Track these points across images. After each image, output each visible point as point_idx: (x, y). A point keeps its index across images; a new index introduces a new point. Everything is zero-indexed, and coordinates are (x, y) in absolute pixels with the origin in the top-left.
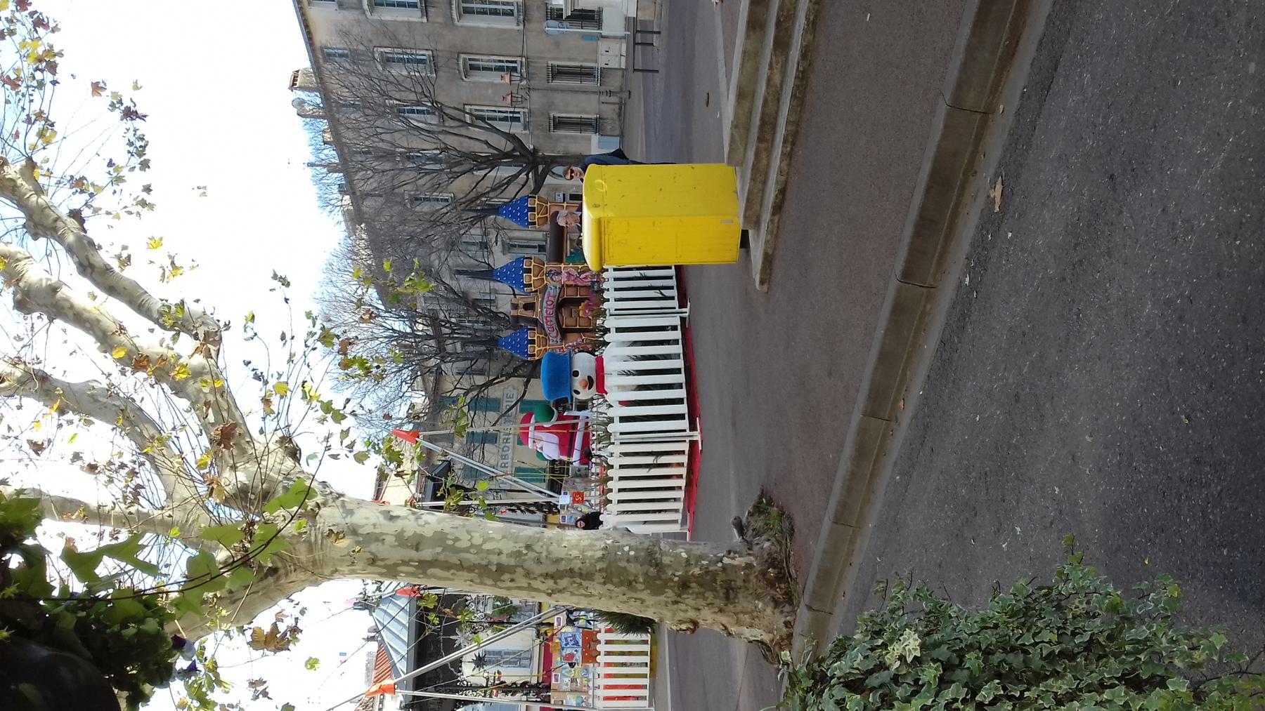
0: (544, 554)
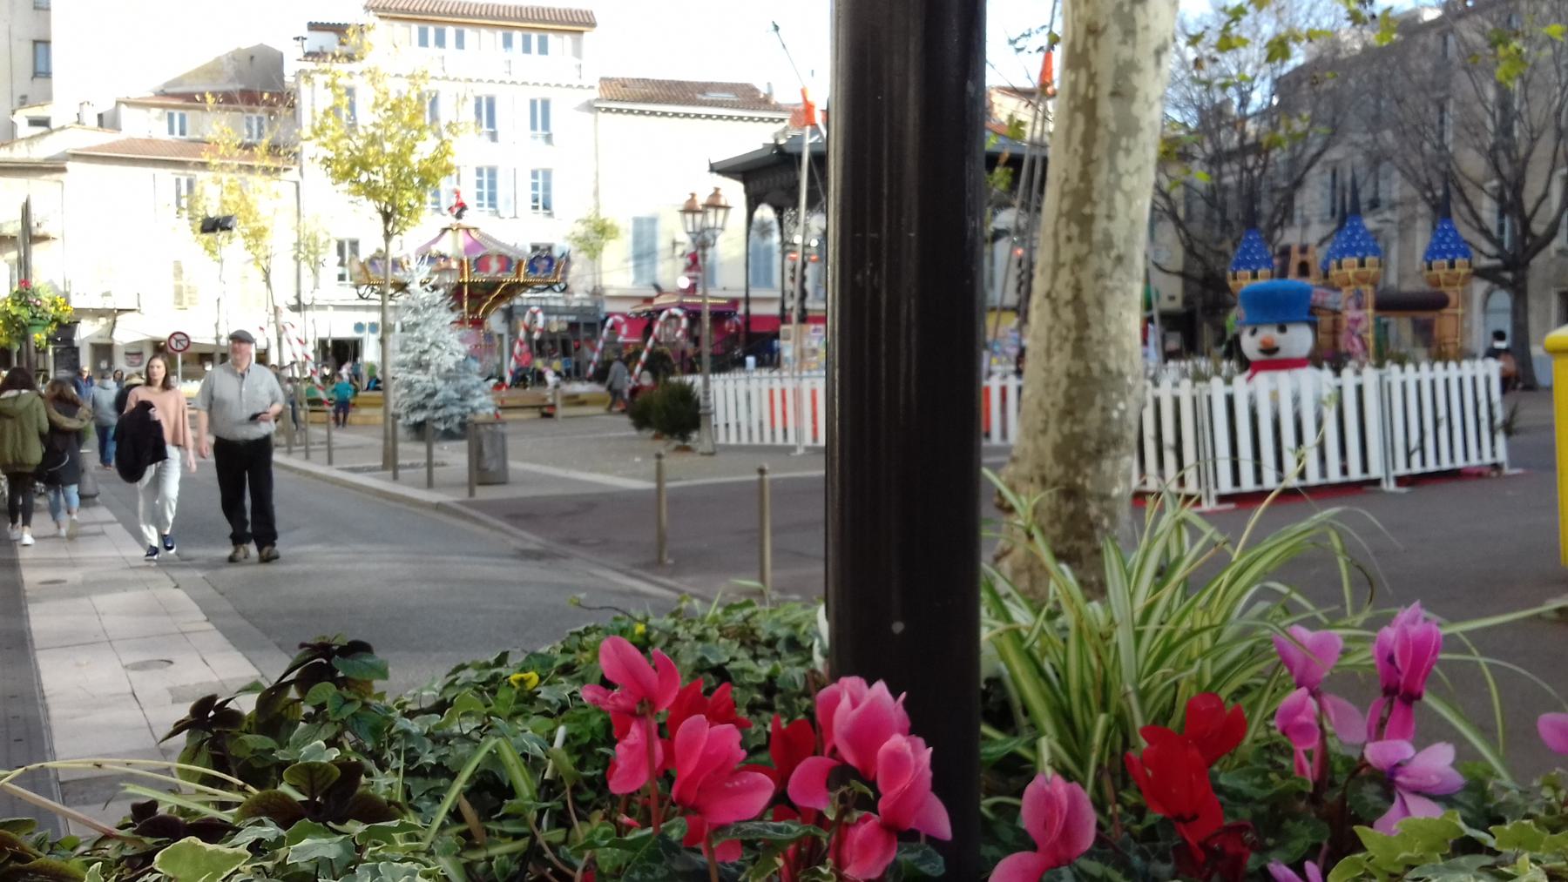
0: (1109, 283)
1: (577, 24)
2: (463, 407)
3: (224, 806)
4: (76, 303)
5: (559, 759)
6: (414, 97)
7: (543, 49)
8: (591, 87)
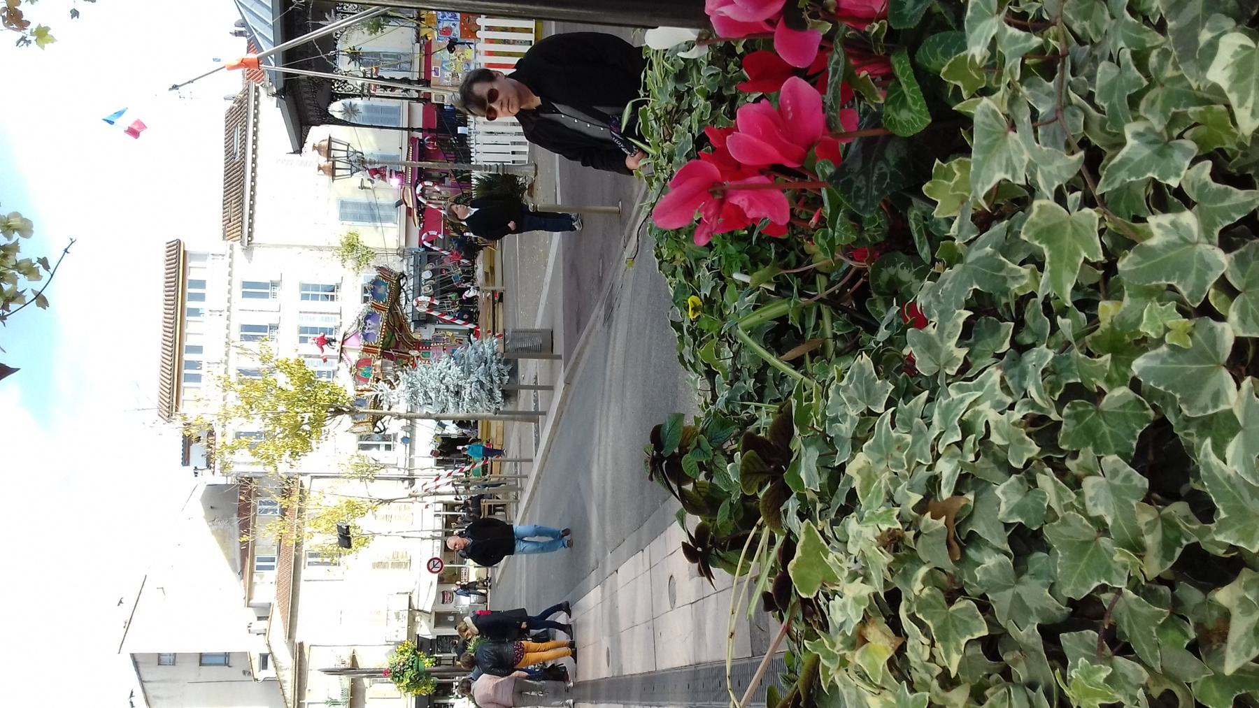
1: (178, 256)
2: (492, 362)
3: (772, 541)
4: (403, 636)
5: (761, 279)
6: (240, 387)
7: (201, 284)
8: (231, 248)
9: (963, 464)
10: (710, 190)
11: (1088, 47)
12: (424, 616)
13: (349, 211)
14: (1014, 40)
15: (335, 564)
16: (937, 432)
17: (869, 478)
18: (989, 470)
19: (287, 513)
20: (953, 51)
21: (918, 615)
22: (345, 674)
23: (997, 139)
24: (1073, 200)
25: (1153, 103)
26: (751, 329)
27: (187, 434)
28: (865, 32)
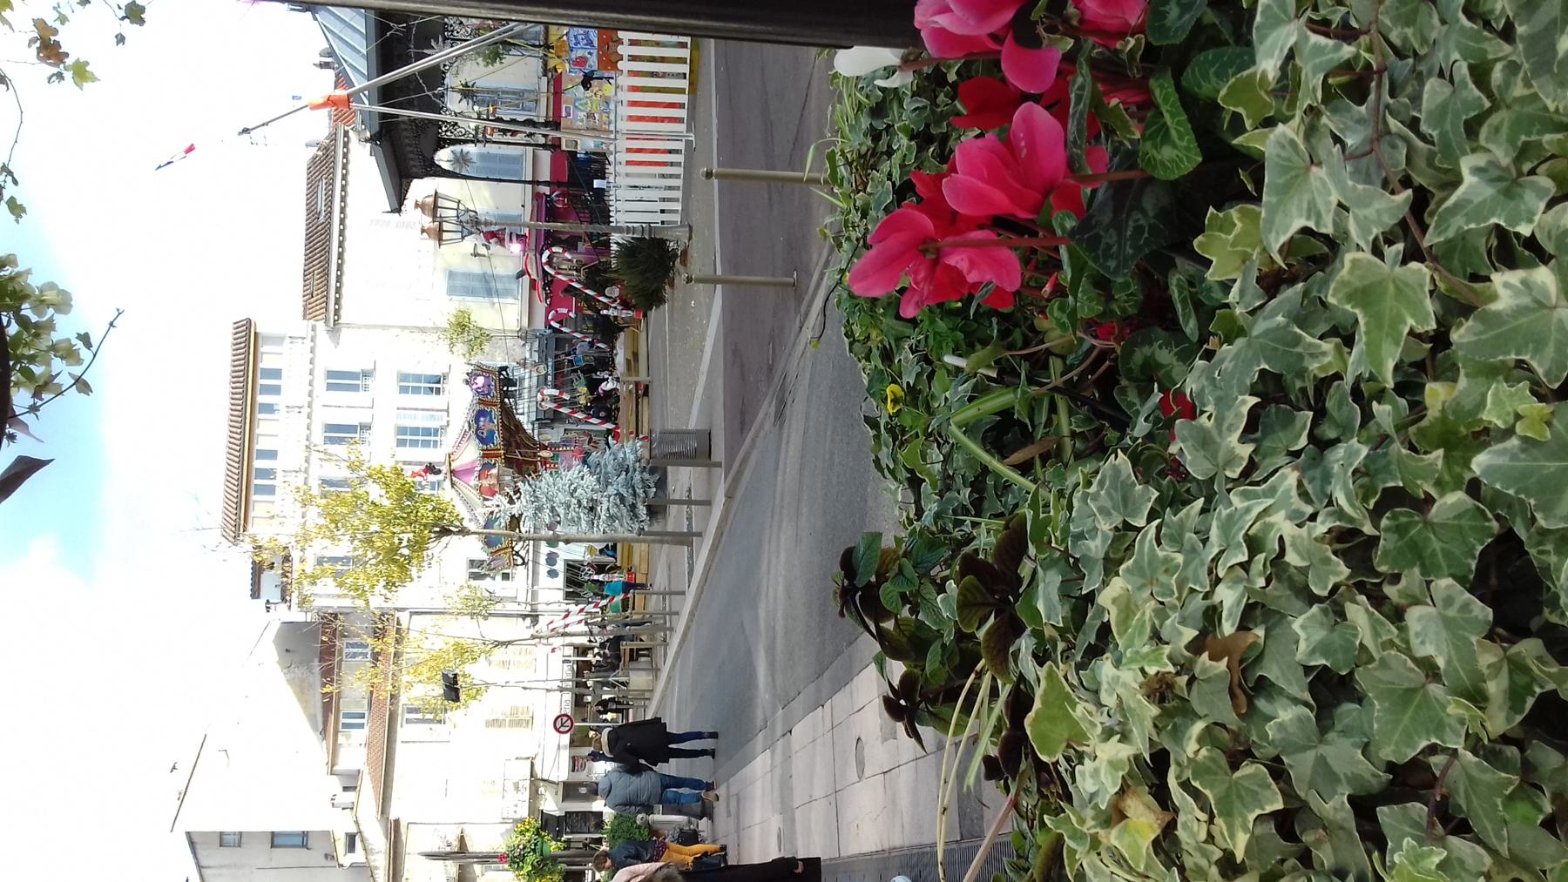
1: (247, 339)
2: (635, 470)
3: (994, 693)
4: (523, 812)
5: (979, 363)
6: (324, 501)
7: (277, 374)
9: (1250, 591)
10: (921, 248)
11: (1411, 61)
12: (550, 787)
13: (461, 284)
14: (1319, 50)
15: (440, 722)
16: (1216, 551)
17: (1128, 608)
18: (1284, 599)
19: (380, 658)
20: (1230, 71)
21: (1193, 783)
22: (452, 859)
23: (1297, 176)
24: (1394, 253)
25: (1497, 130)
26: (966, 425)
27: (258, 559)
28: (1116, 50)
